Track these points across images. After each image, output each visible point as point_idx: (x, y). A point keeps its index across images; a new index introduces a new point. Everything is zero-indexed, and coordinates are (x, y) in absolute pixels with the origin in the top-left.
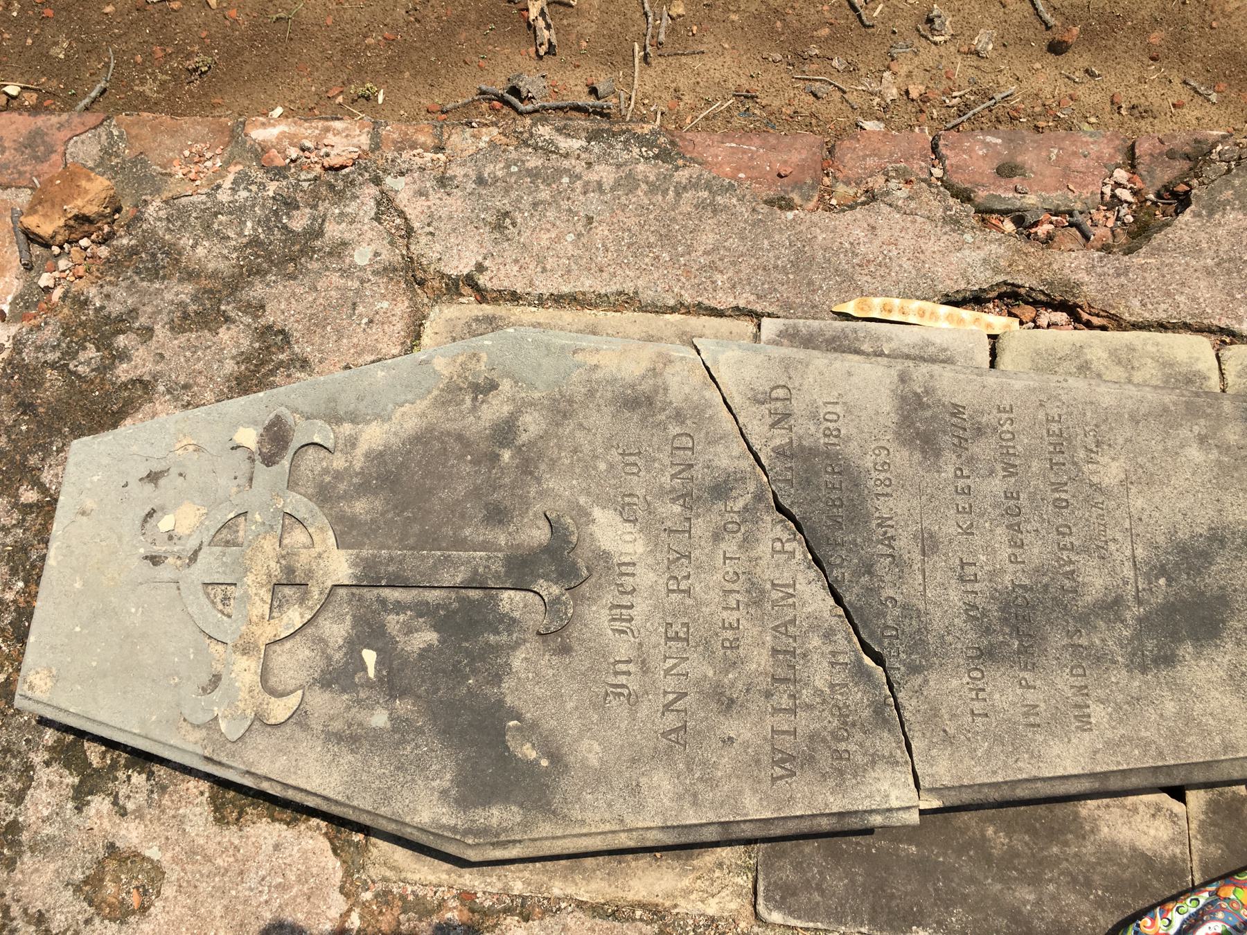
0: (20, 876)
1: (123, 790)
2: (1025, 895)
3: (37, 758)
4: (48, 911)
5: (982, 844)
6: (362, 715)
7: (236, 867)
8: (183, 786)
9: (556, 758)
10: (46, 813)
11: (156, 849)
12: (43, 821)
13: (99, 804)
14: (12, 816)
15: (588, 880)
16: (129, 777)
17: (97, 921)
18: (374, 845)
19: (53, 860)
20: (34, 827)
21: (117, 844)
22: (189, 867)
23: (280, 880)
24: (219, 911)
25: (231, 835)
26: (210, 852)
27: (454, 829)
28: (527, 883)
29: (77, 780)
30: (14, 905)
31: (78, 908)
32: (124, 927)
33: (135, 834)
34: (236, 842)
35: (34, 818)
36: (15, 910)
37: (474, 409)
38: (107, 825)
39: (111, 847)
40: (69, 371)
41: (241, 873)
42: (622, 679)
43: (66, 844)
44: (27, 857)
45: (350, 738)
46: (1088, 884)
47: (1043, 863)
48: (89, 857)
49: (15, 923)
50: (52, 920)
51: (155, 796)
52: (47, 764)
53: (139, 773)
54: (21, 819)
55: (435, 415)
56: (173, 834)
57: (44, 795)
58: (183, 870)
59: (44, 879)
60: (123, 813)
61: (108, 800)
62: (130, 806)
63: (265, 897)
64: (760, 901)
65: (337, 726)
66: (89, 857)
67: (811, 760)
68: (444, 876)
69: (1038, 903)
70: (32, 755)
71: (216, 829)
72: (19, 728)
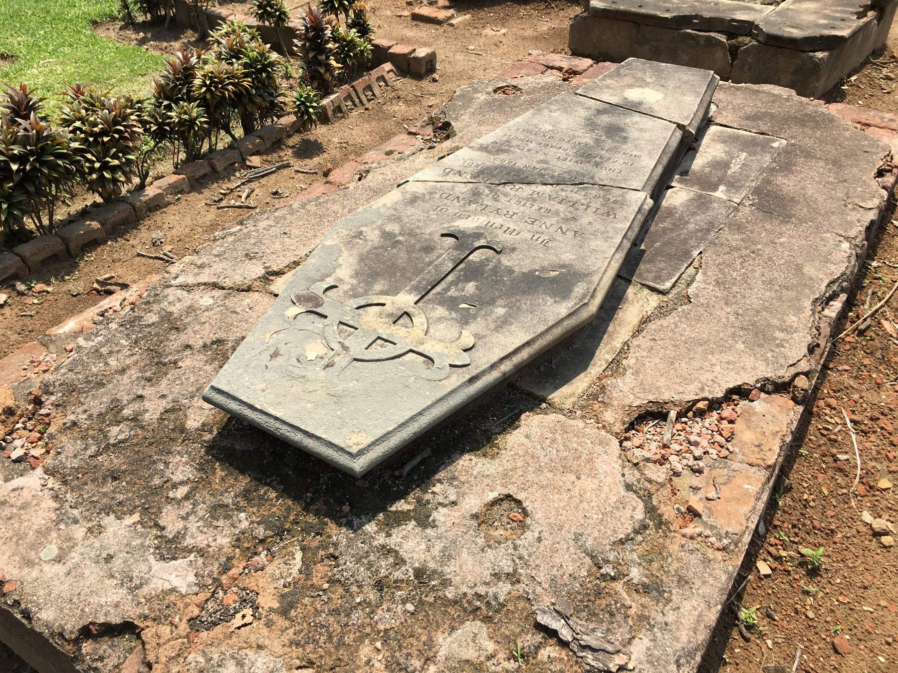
0: (458, 578)
1: (440, 499)
2: (691, 227)
3: (381, 539)
4: (494, 570)
5: (664, 230)
6: (494, 316)
7: (528, 458)
8: (459, 467)
9: (563, 266)
10: (423, 547)
11: (490, 493)
12: (429, 551)
13: (440, 515)
14: (410, 570)
15: (618, 333)
16: (433, 493)
17: (518, 542)
18: (553, 398)
19: (459, 554)
20: (429, 558)
21: (474, 512)
22: (513, 480)
23: (548, 441)
24: (550, 475)
25: (505, 455)
26: (510, 467)
27: (576, 304)
28: (608, 353)
29: (413, 522)
30: (476, 589)
31: (503, 550)
32: (531, 527)
33: (473, 501)
34: (512, 453)
35: (423, 556)
36: (482, 590)
37: (366, 240)
38: (457, 514)
39: (475, 516)
40: (114, 445)
41: (533, 457)
42: (540, 240)
43: (454, 542)
44: (447, 570)
45: (503, 323)
46: (695, 213)
47: (681, 218)
48: (471, 532)
49: (491, 594)
50: (502, 569)
51: (455, 483)
52: (389, 535)
53: (434, 486)
54: (417, 565)
55: (355, 252)
56: (486, 481)
57: (410, 544)
58: (513, 483)
59: (470, 563)
60: (454, 503)
61: (440, 509)
62: (453, 498)
63: (555, 452)
64: (658, 286)
65: (492, 326)
66: (471, 532)
67: (612, 209)
68: (587, 379)
69: (696, 224)
70: (375, 543)
71: (497, 460)
72: (349, 547)
